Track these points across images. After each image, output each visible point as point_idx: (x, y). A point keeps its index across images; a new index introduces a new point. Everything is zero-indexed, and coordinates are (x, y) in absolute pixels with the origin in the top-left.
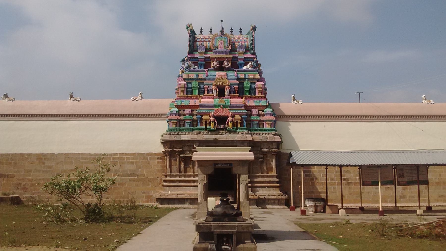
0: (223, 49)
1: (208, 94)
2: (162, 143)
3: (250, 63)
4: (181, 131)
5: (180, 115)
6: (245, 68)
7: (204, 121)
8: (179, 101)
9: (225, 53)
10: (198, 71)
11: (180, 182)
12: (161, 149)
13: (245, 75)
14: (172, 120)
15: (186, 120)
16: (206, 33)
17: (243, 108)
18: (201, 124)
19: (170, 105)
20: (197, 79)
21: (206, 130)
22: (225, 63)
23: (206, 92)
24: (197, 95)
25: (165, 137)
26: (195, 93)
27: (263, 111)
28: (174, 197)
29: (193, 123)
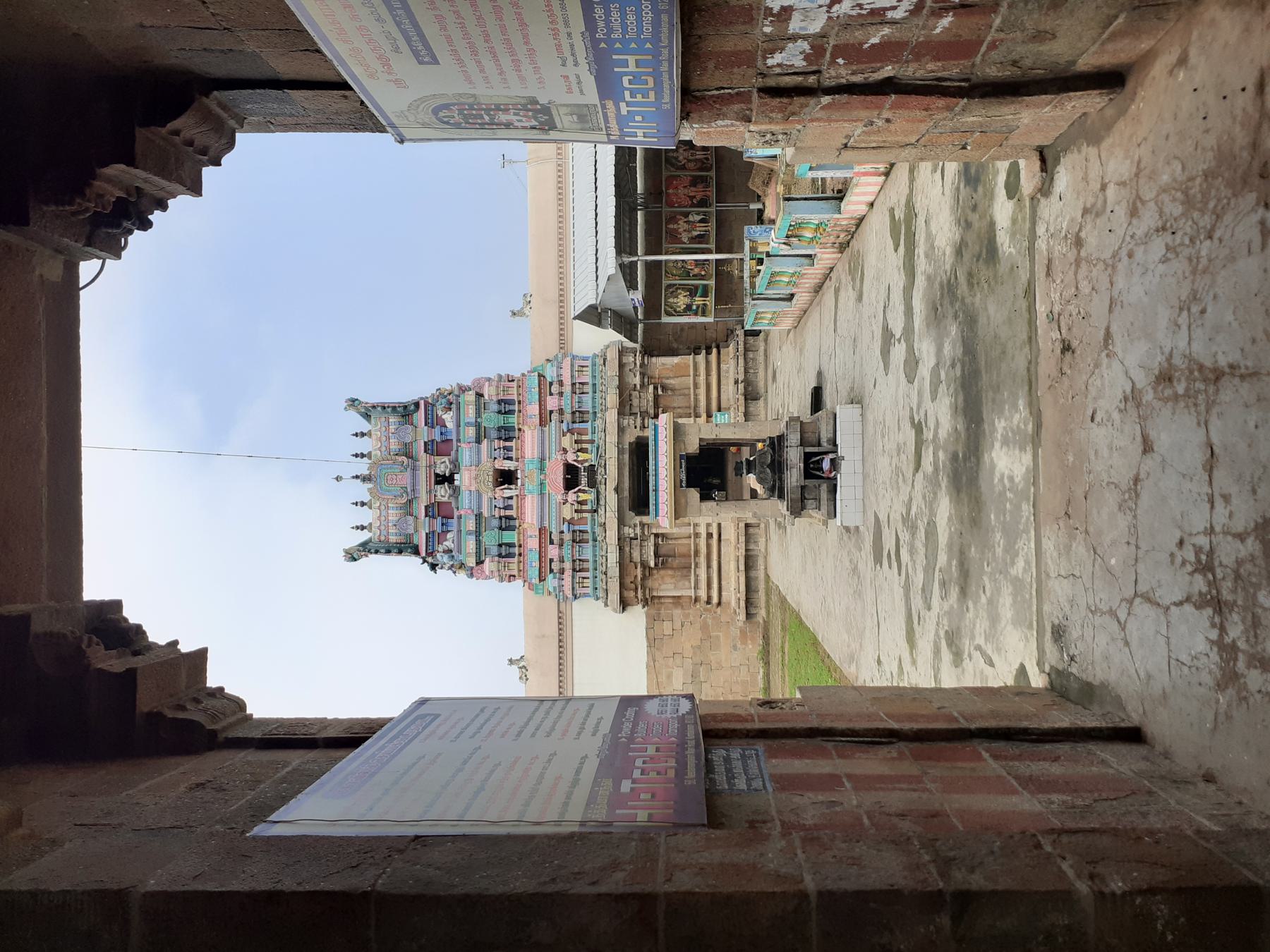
0: (408, 473)
3: (440, 413)
5: (562, 571)
6: (450, 425)
7: (575, 515)
9: (414, 469)
10: (460, 531)
11: (709, 566)
12: (638, 614)
13: (468, 424)
16: (366, 516)
17: (546, 429)
18: (582, 521)
20: (478, 534)
21: (595, 511)
22: (441, 469)
23: (508, 513)
24: (515, 533)
26: (509, 537)
27: (551, 560)
28: (742, 580)
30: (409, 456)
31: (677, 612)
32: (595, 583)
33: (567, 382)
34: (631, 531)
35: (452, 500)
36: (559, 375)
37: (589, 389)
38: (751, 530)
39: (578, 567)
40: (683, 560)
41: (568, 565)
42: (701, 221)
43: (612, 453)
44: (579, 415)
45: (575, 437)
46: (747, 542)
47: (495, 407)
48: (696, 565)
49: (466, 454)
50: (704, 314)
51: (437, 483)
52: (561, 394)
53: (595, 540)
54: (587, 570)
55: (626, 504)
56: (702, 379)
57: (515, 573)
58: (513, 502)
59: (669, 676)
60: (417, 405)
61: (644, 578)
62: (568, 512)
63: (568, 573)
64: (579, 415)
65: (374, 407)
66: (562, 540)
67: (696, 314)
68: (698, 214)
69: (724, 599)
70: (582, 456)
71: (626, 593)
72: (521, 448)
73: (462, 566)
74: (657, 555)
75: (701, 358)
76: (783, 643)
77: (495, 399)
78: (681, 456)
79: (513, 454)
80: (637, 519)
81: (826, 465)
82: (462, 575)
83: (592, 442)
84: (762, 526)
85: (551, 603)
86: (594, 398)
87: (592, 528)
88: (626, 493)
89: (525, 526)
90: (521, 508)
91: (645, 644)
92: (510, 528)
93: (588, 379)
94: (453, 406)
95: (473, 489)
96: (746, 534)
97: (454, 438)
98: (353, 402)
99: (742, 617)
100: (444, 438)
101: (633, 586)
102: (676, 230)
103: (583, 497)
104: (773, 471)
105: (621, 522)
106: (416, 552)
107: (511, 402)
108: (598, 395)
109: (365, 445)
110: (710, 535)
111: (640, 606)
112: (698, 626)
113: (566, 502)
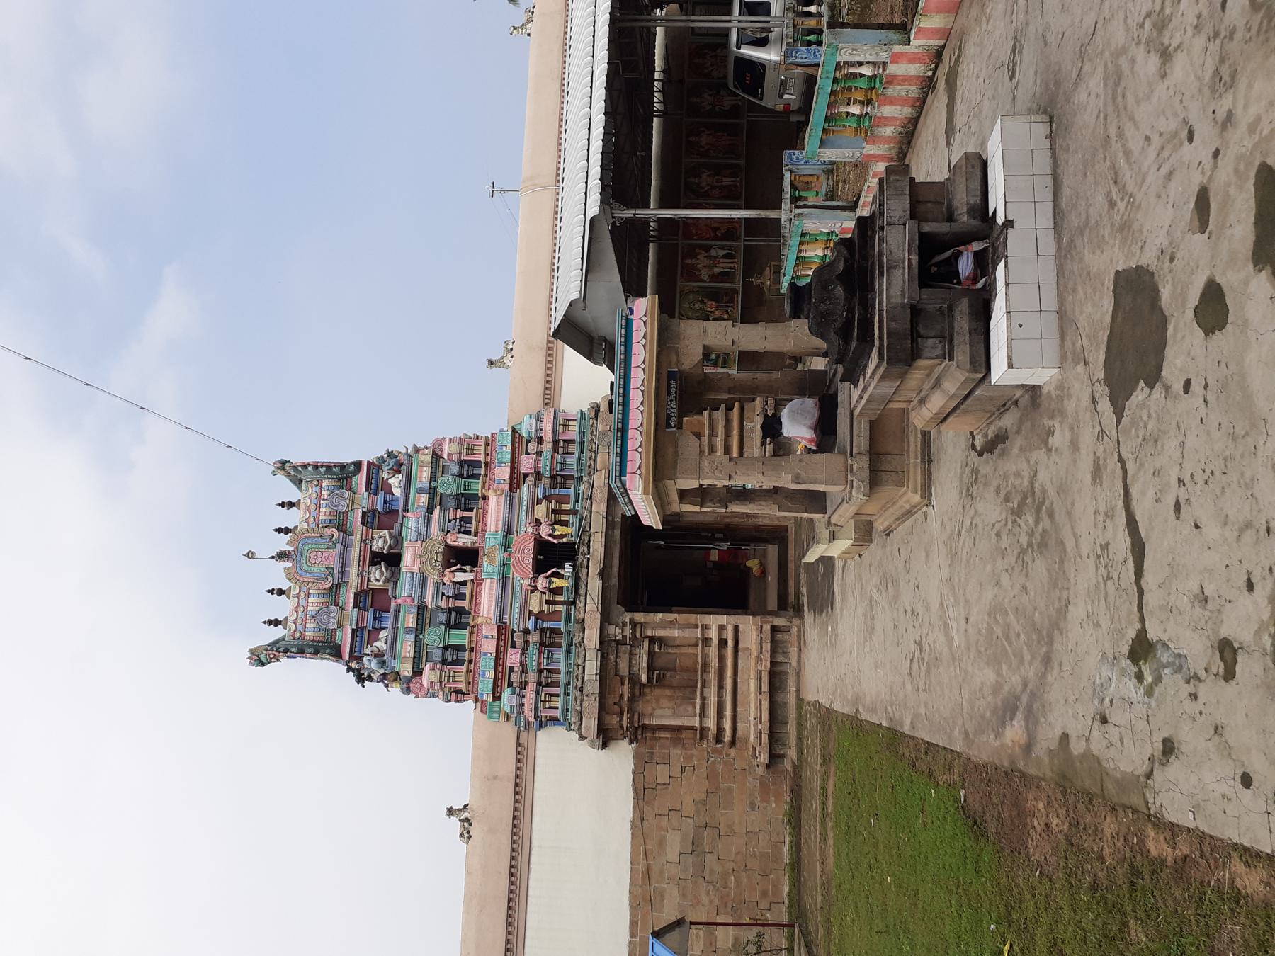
0: (337, 552)
1: (468, 596)
2: (604, 745)
3: (386, 476)
4: (574, 682)
5: (523, 685)
6: (397, 492)
7: (545, 608)
8: (481, 686)
9: (346, 546)
10: (396, 629)
11: (721, 686)
12: (622, 755)
13: (420, 491)
14: (536, 708)
15: (539, 664)
16: (282, 609)
17: (516, 495)
18: (554, 616)
19: (491, 717)
20: (419, 630)
21: (573, 603)
22: (378, 545)
23: (459, 603)
24: (466, 633)
25: (587, 729)
26: (460, 637)
27: (511, 669)
28: (766, 705)
29: (549, 640)
30: (342, 528)
31: (676, 752)
32: (566, 702)
33: (548, 436)
34: (618, 631)
35: (389, 587)
36: (539, 430)
37: (575, 448)
38: (779, 636)
39: (546, 678)
40: (686, 676)
41: (531, 677)
42: (725, 257)
43: (598, 526)
44: (559, 478)
45: (552, 506)
46: (773, 652)
47: (455, 469)
48: (704, 684)
49: (411, 525)
50: (725, 365)
51: (373, 563)
52: (539, 454)
53: (570, 643)
54: (557, 685)
55: (614, 596)
56: (719, 440)
57: (462, 686)
58: (467, 590)
59: (661, 843)
60: (358, 465)
61: (632, 699)
62: (535, 604)
63: (531, 687)
64: (559, 478)
65: (304, 466)
66: (526, 643)
67: (715, 365)
68: (722, 248)
69: (740, 733)
70: (560, 530)
71: (607, 719)
72: (482, 520)
73: (397, 676)
74: (651, 667)
75: (719, 415)
76: (825, 782)
77: (455, 458)
78: (671, 376)
79: (472, 527)
80: (627, 617)
81: (965, 265)
82: (396, 689)
83: (574, 512)
84: (794, 630)
85: (509, 731)
86: (580, 459)
87: (567, 626)
88: (615, 581)
89: (479, 620)
90: (475, 597)
91: (631, 794)
92: (461, 626)
93: (575, 436)
94: (404, 468)
95: (416, 570)
96: (773, 641)
97: (400, 507)
98: (283, 465)
99: (764, 758)
100: (388, 507)
101: (617, 708)
102: (694, 266)
103: (557, 583)
104: (849, 289)
105: (606, 619)
106: (337, 654)
107: (476, 464)
108: (586, 455)
109: (292, 518)
110: (723, 643)
111: (626, 741)
112: (703, 773)
113: (534, 589)
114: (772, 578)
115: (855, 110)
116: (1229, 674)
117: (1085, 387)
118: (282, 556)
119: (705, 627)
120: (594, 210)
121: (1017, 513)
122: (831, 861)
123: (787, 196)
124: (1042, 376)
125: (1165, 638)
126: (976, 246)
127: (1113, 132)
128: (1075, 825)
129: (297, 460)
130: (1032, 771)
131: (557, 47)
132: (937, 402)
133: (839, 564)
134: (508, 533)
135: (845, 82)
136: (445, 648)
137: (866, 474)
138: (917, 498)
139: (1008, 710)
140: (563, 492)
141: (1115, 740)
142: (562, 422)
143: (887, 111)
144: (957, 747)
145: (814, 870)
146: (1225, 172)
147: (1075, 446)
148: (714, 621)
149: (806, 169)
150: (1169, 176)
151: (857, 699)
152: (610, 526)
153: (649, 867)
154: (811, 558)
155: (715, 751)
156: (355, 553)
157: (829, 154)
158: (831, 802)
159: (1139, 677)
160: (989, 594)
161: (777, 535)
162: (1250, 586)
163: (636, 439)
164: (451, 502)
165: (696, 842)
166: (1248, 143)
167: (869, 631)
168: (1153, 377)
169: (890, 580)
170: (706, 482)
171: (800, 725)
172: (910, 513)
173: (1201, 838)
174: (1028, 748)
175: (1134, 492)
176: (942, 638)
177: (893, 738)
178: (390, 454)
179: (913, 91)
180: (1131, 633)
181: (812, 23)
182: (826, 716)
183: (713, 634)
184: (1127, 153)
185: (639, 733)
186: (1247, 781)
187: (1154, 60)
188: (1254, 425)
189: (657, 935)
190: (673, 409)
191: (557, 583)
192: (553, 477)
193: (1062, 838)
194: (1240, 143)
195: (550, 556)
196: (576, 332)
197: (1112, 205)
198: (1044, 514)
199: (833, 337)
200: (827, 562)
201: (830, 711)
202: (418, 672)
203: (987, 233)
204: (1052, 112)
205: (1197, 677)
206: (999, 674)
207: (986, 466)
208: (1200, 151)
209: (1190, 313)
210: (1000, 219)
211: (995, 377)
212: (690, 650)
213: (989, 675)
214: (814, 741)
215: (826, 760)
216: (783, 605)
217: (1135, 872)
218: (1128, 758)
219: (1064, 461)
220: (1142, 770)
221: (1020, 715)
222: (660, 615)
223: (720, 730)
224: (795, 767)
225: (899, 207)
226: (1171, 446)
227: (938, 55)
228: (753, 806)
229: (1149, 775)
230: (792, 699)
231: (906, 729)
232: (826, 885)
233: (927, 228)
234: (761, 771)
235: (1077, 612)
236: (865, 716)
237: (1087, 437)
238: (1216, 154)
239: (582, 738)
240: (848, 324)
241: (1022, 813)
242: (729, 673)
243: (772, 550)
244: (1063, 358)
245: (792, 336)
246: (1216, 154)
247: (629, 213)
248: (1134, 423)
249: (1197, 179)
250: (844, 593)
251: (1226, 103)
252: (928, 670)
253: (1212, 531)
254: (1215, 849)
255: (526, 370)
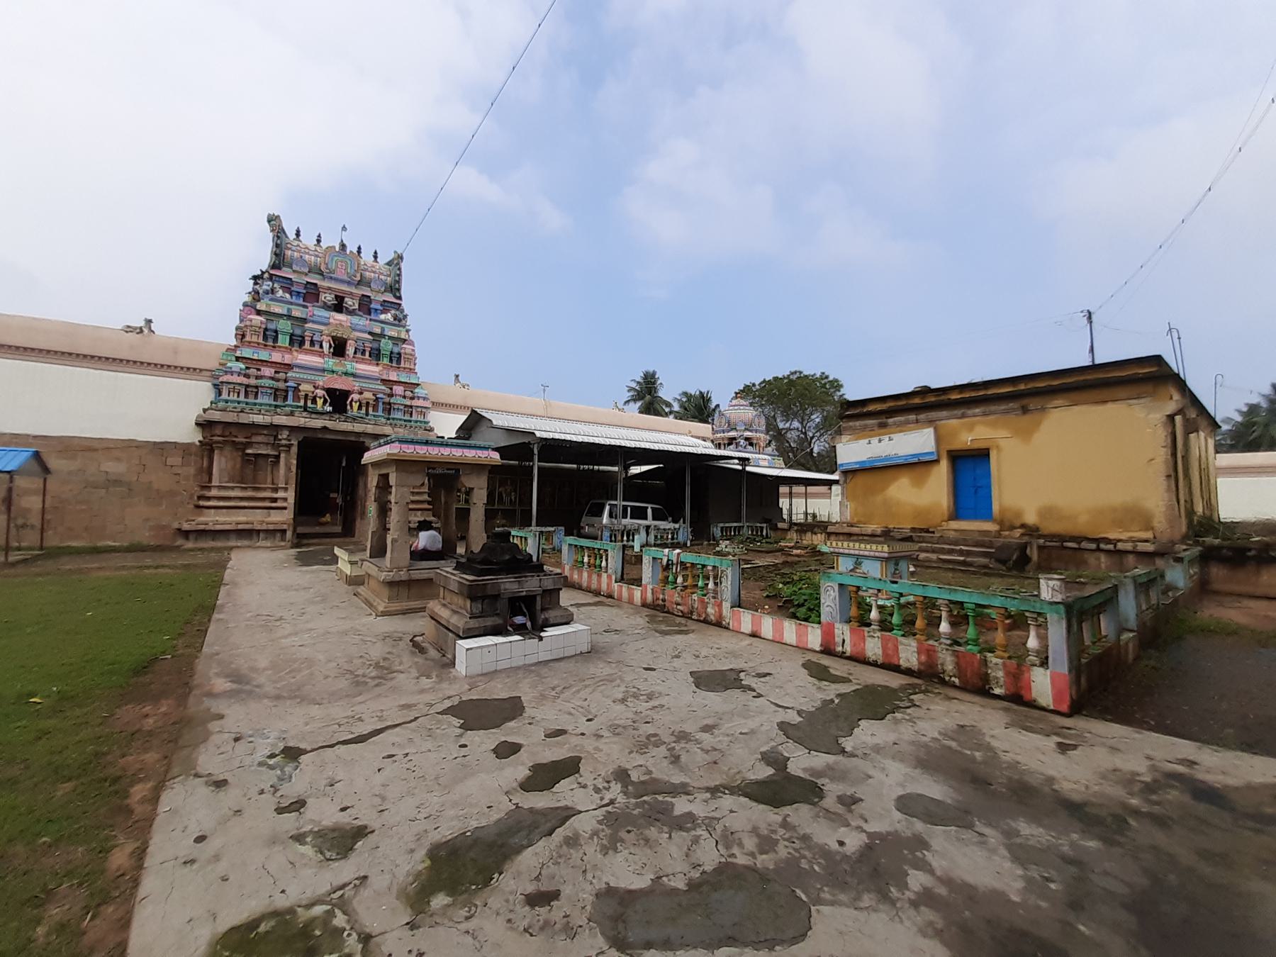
0: (345, 278)
2: (197, 424)
6: (383, 317)
9: (349, 283)
10: (291, 304)
11: (242, 499)
13: (383, 329)
18: (296, 398)
21: (305, 410)
22: (348, 301)
26: (284, 341)
30: (359, 283)
32: (232, 402)
33: (415, 403)
37: (407, 417)
38: (279, 535)
41: (253, 381)
43: (358, 428)
44: (389, 408)
47: (396, 350)
49: (361, 321)
53: (276, 406)
54: (246, 396)
55: (309, 434)
57: (247, 338)
58: (317, 348)
59: (118, 459)
60: (400, 298)
62: (305, 387)
63: (245, 381)
64: (389, 408)
70: (356, 406)
72: (363, 361)
75: (426, 497)
78: (458, 471)
79: (359, 355)
80: (295, 443)
81: (519, 620)
82: (247, 298)
83: (367, 414)
85: (213, 364)
88: (320, 436)
92: (292, 342)
93: (414, 418)
98: (401, 257)
99: (186, 527)
103: (320, 402)
105: (292, 429)
106: (274, 266)
107: (399, 362)
109: (367, 257)
110: (275, 500)
114: (318, 529)
115: (586, 559)
116: (280, 811)
117: (456, 691)
118: (343, 246)
119: (286, 489)
120: (538, 434)
121: (377, 666)
122: (101, 574)
123: (543, 529)
124: (461, 667)
125: (302, 766)
126: (529, 624)
127: (587, 683)
128: (150, 733)
129: (403, 265)
130: (191, 700)
131: (604, 421)
132: (444, 613)
133: (333, 568)
134: (354, 375)
135: (597, 554)
136: (276, 331)
137: (397, 579)
138: (381, 609)
139: (237, 677)
140: (380, 408)
141: (222, 750)
142: (423, 411)
143: (585, 575)
144: (205, 649)
145: (91, 563)
146: (575, 740)
147: (422, 691)
148: (291, 495)
149: (556, 540)
150: (570, 714)
151: (235, 584)
152: (358, 434)
153: (96, 450)
154: (337, 551)
155: (192, 496)
156: (344, 288)
157: (565, 549)
158: (152, 571)
159: (272, 756)
160: (321, 657)
161: (348, 531)
162: (343, 810)
163: (422, 450)
164: (375, 345)
165: (117, 482)
166: (590, 749)
167: (287, 588)
168: (466, 727)
169: (324, 599)
170: (394, 489)
171: (212, 549)
172: (370, 605)
173: (149, 820)
174: (211, 695)
175: (398, 729)
176: (286, 632)
177: (208, 609)
178: (405, 316)
179: (594, 586)
180: (302, 746)
181: (619, 538)
182: (222, 566)
183: (281, 494)
184: (578, 691)
185: (207, 448)
186: (200, 839)
187: (620, 696)
188: (446, 787)
189: (37, 456)
190: (439, 471)
191: (320, 402)
192: (390, 404)
193: (137, 727)
194: (589, 744)
195: (338, 400)
196: (474, 423)
197: (553, 689)
198: (377, 681)
199: (482, 555)
200: (335, 560)
201: (225, 568)
202: (259, 313)
203: (535, 629)
204: (592, 653)
205: (276, 791)
206: (265, 669)
207: (405, 644)
208: (584, 726)
209: (503, 739)
210: (543, 634)
211: (460, 642)
212: (269, 480)
213: (263, 662)
214: (200, 559)
215: (186, 567)
216: (300, 537)
217: (116, 780)
218: (209, 760)
219: (414, 688)
220: (199, 769)
221: (234, 686)
222: (295, 462)
223: (209, 498)
224: (178, 547)
225: (548, 584)
226: (429, 745)
227: (610, 596)
228: (147, 520)
229: (197, 776)
230: (232, 543)
231: (216, 616)
232: (80, 571)
233: (538, 598)
234: (176, 525)
235: (315, 711)
236: (223, 590)
237: (428, 698)
238: (583, 734)
239: (205, 410)
240: (491, 563)
241: (156, 699)
242: (222, 504)
243: (338, 529)
244: (471, 677)
245: (478, 537)
246: (583, 734)
247: (536, 451)
248: (439, 722)
249: (570, 728)
250: (312, 572)
251: (606, 734)
252: (262, 626)
253: (378, 779)
254: (142, 829)
255: (454, 394)
